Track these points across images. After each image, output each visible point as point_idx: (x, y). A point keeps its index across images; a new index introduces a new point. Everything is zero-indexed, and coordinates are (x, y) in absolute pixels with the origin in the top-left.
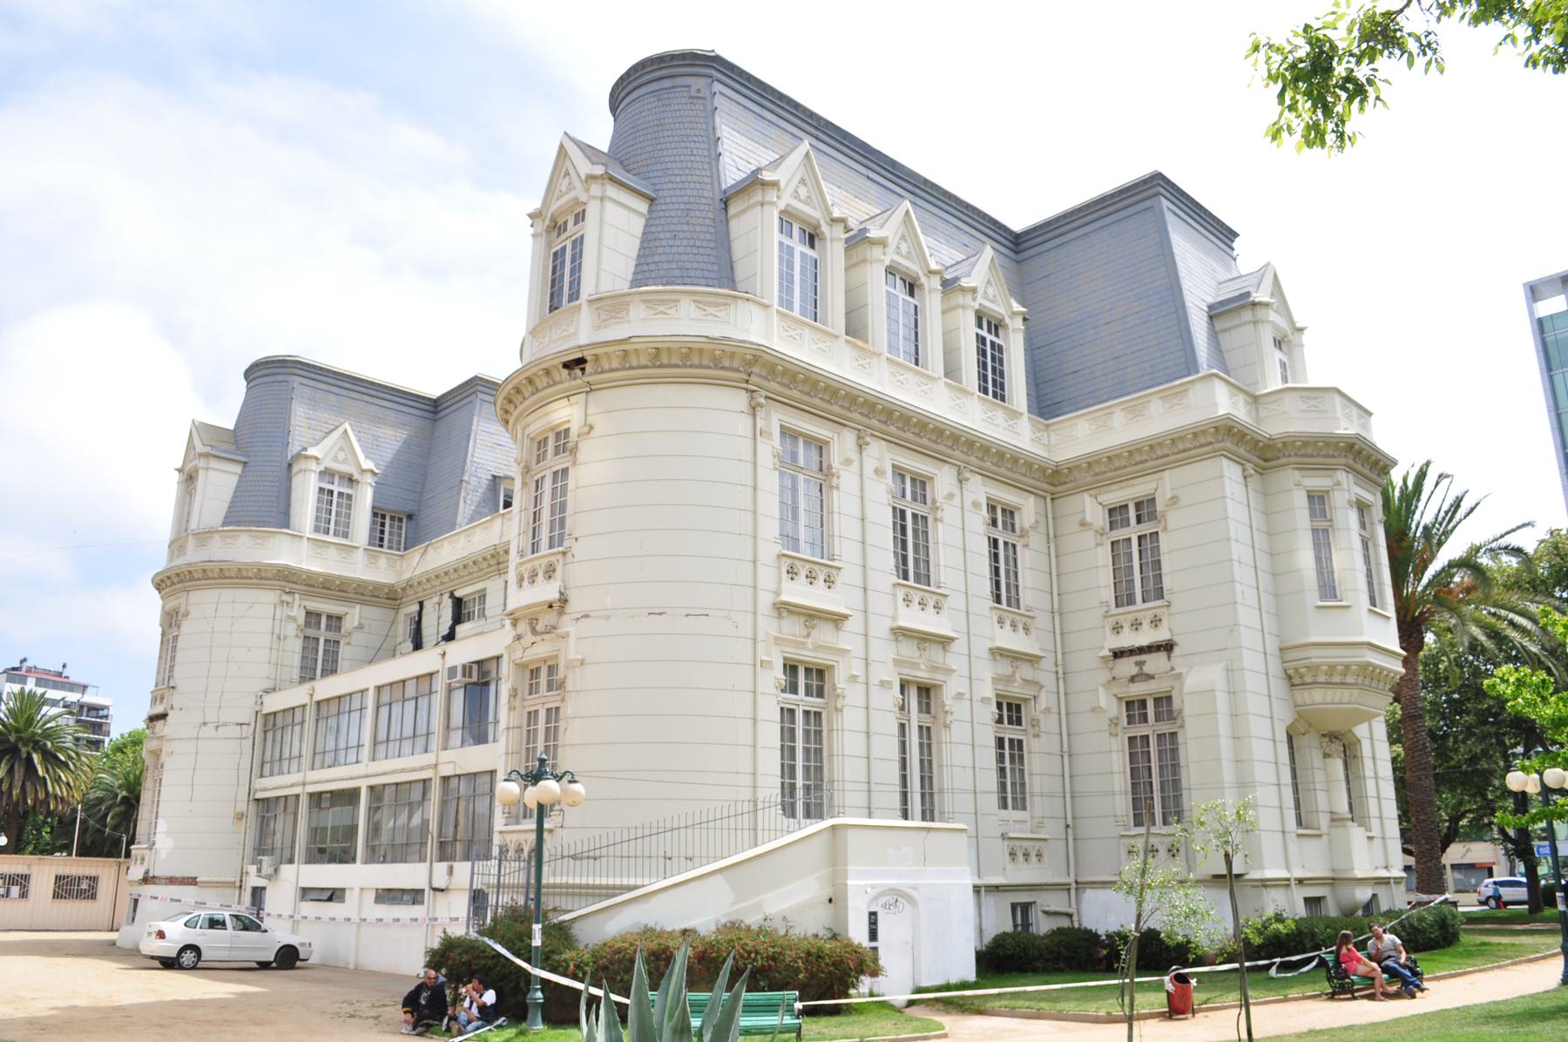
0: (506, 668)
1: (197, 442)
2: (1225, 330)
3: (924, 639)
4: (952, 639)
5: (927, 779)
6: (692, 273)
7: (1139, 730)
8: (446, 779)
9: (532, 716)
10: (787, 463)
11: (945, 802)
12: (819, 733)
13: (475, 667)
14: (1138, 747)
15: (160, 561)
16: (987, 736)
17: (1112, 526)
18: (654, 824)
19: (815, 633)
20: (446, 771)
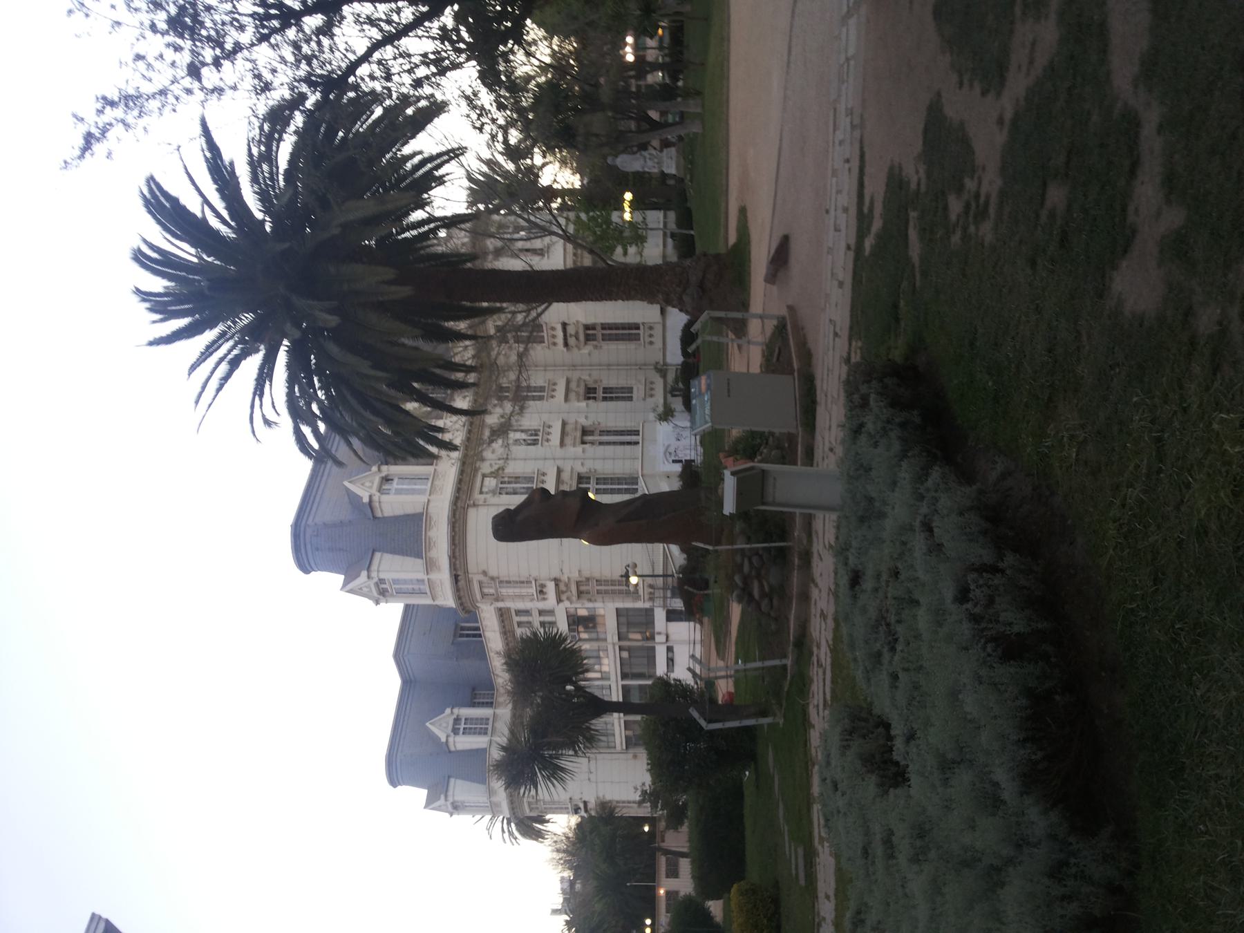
5: (621, 433)
8: (620, 639)
9: (599, 592)
14: (606, 338)
20: (616, 638)
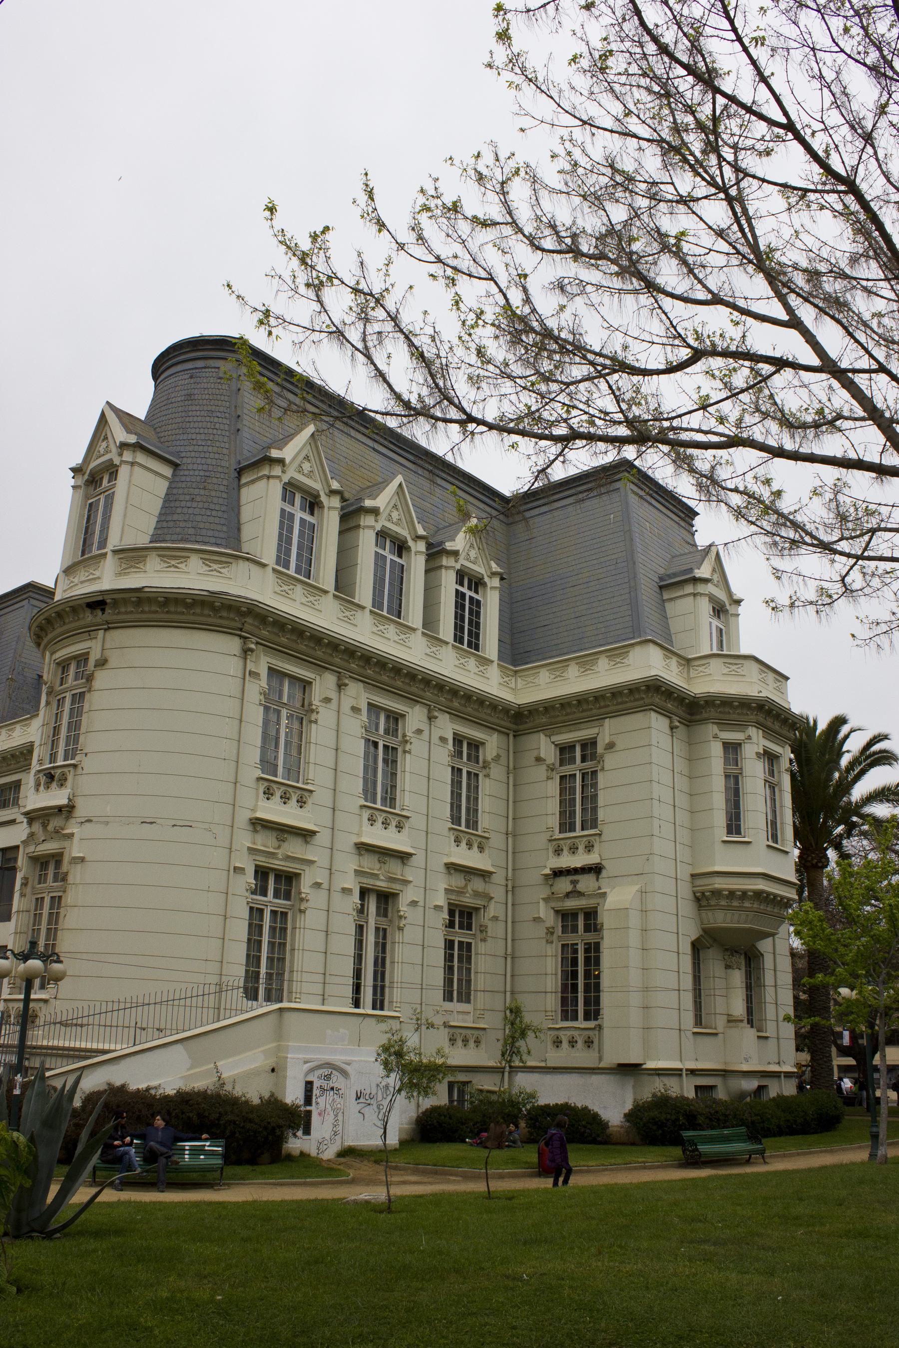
0: (22, 861)
2: (671, 599)
3: (384, 853)
4: (410, 855)
5: (380, 974)
6: (204, 532)
7: (571, 939)
9: (40, 901)
11: (395, 994)
12: (284, 930)
16: (437, 939)
18: (129, 1000)
19: (285, 845)
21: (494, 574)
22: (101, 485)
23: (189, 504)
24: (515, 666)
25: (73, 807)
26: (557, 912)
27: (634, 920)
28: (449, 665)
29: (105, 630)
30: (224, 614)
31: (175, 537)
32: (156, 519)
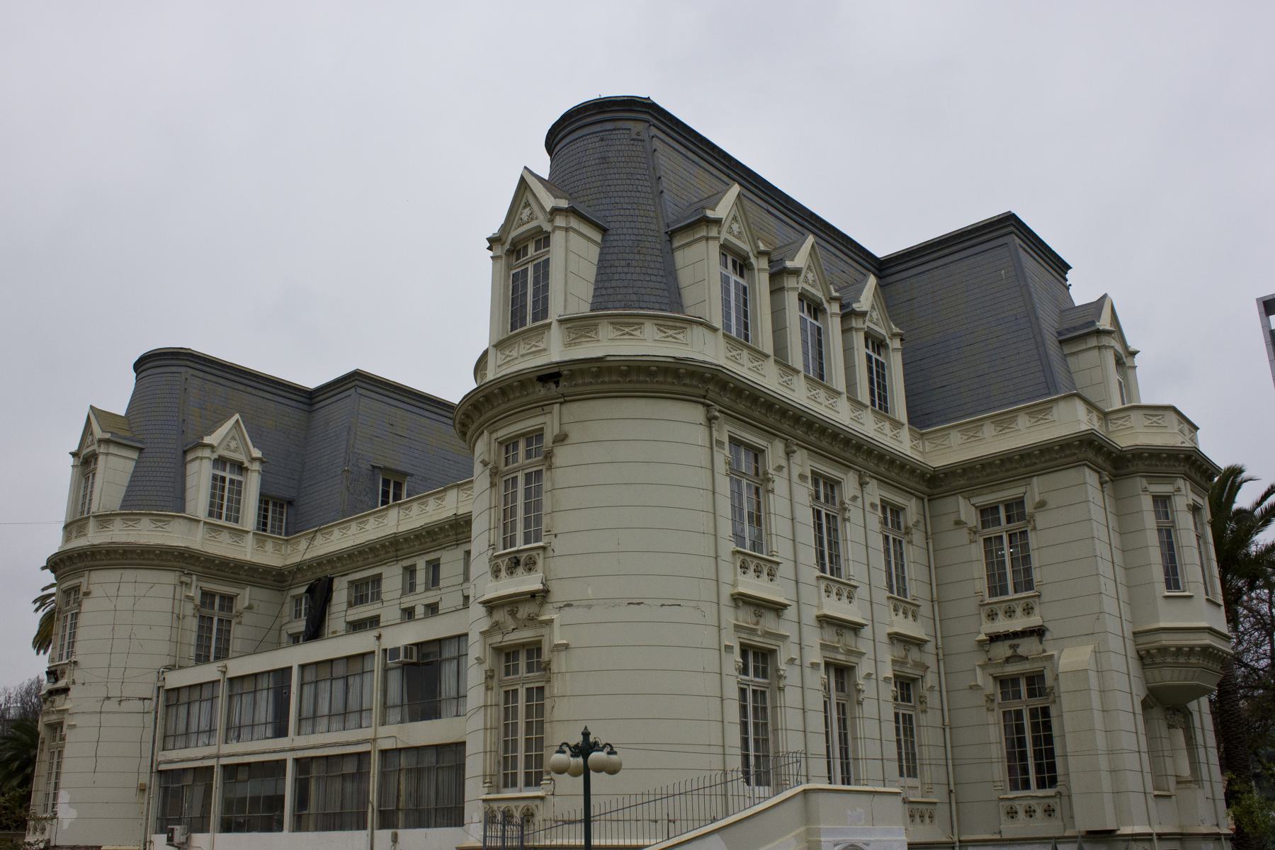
1: (96, 427)
2: (1073, 354)
6: (646, 298)
7: (1014, 705)
8: (384, 753)
9: (511, 695)
10: (734, 472)
13: (415, 649)
14: (1013, 724)
15: (54, 542)
16: (889, 711)
17: (985, 524)
18: (658, 791)
19: (762, 620)
21: (894, 335)
22: (525, 254)
23: (626, 270)
24: (921, 428)
25: (548, 591)
26: (995, 678)
27: (1094, 681)
28: (868, 427)
29: (561, 403)
30: (687, 381)
31: (617, 304)
32: (592, 287)
